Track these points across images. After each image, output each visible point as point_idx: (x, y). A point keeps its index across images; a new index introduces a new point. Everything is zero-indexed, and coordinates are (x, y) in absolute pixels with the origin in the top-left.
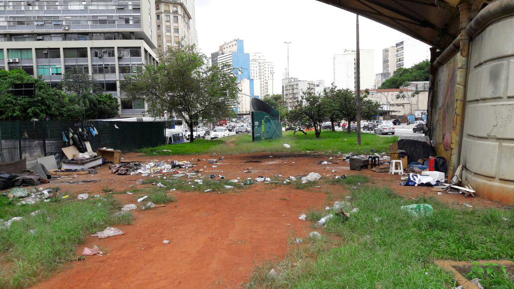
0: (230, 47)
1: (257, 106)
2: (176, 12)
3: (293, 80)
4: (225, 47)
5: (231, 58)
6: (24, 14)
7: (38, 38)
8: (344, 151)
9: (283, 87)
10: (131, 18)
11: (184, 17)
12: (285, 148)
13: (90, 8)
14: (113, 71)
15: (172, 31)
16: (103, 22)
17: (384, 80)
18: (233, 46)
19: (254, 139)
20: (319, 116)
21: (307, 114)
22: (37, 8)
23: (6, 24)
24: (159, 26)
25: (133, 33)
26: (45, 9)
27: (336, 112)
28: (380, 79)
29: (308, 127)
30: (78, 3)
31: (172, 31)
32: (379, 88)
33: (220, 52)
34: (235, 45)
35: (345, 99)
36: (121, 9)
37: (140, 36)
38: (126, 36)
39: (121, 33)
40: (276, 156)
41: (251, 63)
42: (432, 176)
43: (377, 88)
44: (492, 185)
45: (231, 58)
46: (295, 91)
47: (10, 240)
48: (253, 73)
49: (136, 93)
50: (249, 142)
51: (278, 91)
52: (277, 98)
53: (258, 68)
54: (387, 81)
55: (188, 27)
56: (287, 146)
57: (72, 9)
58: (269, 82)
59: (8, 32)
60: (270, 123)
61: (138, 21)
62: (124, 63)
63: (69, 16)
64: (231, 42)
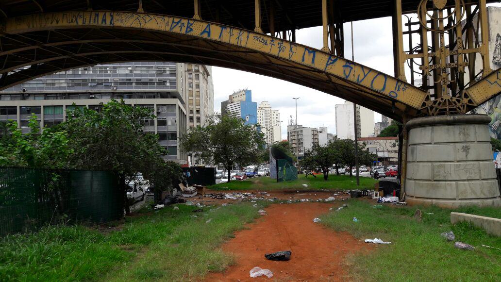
0: (239, 96)
1: (275, 154)
2: (198, 71)
3: (298, 127)
5: (240, 106)
6: (81, 77)
7: (91, 96)
8: (346, 189)
9: (288, 133)
10: (168, 81)
11: (203, 75)
12: (304, 186)
13: (135, 72)
14: (152, 124)
15: (194, 86)
16: (145, 83)
17: (383, 128)
18: (241, 95)
19: (278, 180)
20: (326, 162)
21: (317, 161)
22: (91, 72)
23: (65, 85)
25: (169, 93)
26: (98, 73)
27: (340, 159)
28: (379, 127)
29: (318, 172)
30: (125, 69)
31: (194, 86)
32: (378, 136)
33: (230, 101)
34: (244, 94)
35: (347, 149)
36: (159, 74)
37: (175, 96)
38: (164, 95)
39: (160, 92)
40: (301, 192)
41: (258, 110)
42: (394, 199)
43: (376, 136)
44: (424, 202)
45: (240, 106)
46: (300, 137)
49: (192, 144)
50: (274, 182)
51: (285, 137)
52: (285, 144)
54: (385, 129)
55: (207, 83)
56: (306, 185)
57: (120, 73)
58: (274, 128)
59: (67, 92)
61: (174, 84)
62: (161, 117)
63: (117, 78)
64: (240, 92)
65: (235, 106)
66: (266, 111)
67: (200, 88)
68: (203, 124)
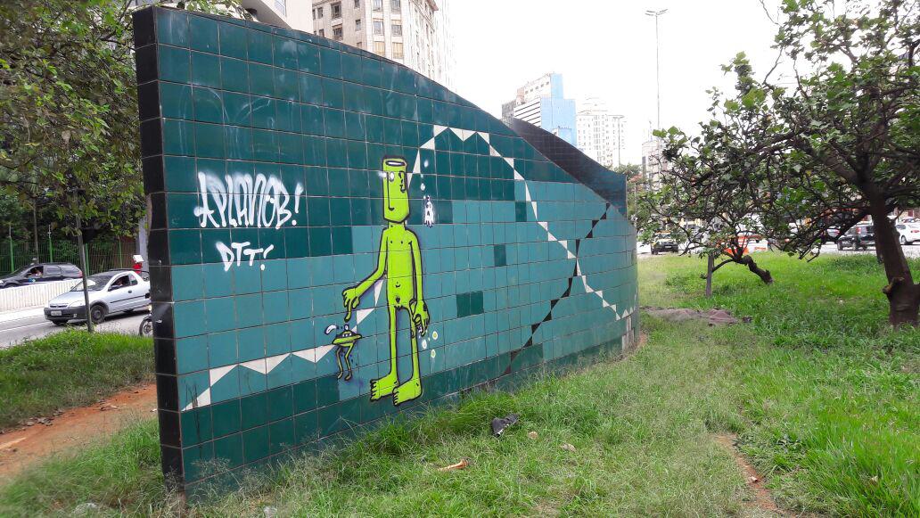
4: (528, 89)
5: (539, 110)
15: (388, 31)
24: (358, 21)
34: (548, 83)
45: (539, 110)
47: (788, 199)
48: (582, 138)
52: (630, 172)
53: (592, 126)
60: (507, 208)
65: (530, 108)
66: (596, 117)
67: (403, 14)
68: (328, 451)
